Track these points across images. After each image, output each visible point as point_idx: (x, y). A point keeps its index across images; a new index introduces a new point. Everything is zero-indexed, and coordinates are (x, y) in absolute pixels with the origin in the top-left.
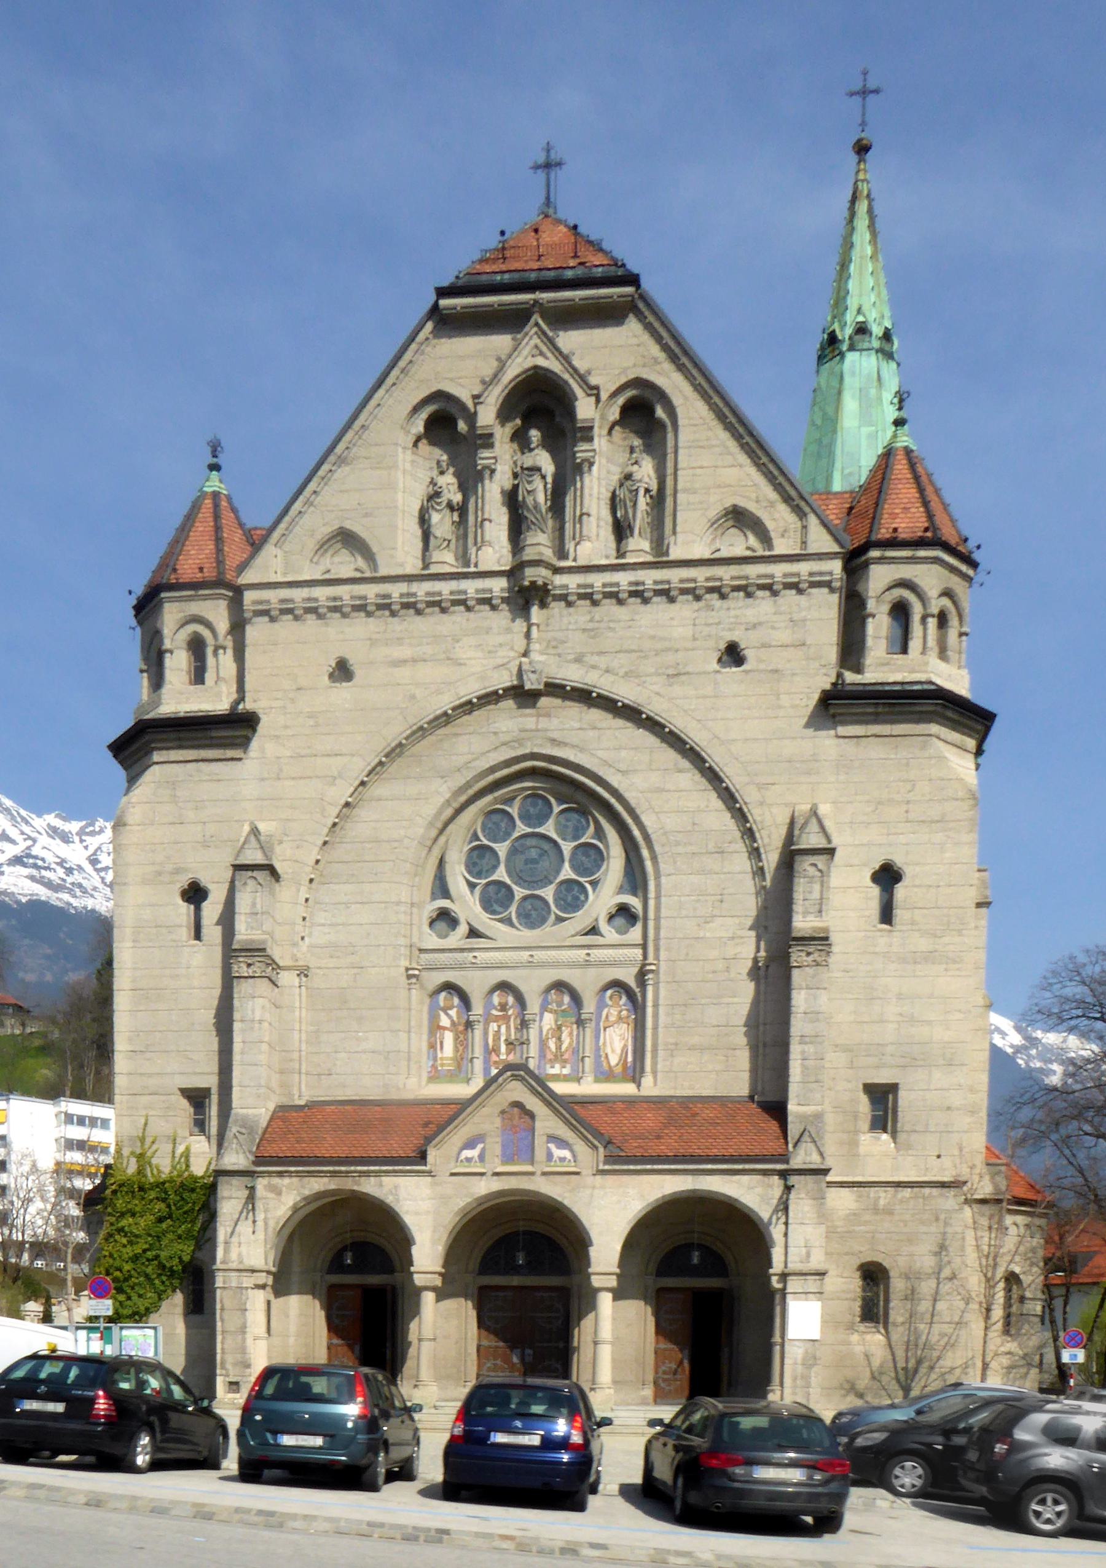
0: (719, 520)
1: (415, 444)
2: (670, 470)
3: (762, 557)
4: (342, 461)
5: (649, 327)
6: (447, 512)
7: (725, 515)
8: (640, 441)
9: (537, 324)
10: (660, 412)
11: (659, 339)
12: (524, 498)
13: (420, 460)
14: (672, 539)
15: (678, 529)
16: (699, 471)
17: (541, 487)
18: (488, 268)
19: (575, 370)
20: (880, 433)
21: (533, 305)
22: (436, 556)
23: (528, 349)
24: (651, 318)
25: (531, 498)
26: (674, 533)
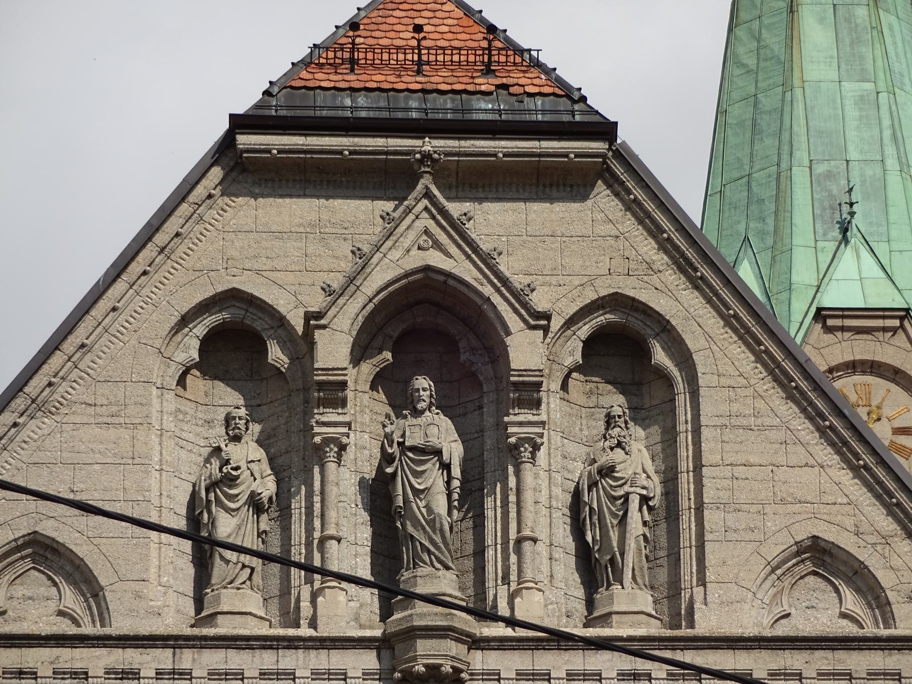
0: (784, 562)
1: (182, 382)
2: (685, 461)
3: (877, 639)
4: (37, 407)
5: (632, 207)
6: (247, 513)
7: (798, 553)
8: (621, 399)
9: (428, 195)
10: (660, 356)
11: (655, 231)
12: (406, 500)
13: (188, 407)
14: (698, 592)
15: (710, 575)
16: (740, 471)
17: (440, 485)
18: (324, 79)
19: (505, 282)
20: (883, 97)
21: (421, 162)
22: (228, 600)
23: (411, 235)
24: (639, 193)
25: (422, 504)
26: (702, 582)
